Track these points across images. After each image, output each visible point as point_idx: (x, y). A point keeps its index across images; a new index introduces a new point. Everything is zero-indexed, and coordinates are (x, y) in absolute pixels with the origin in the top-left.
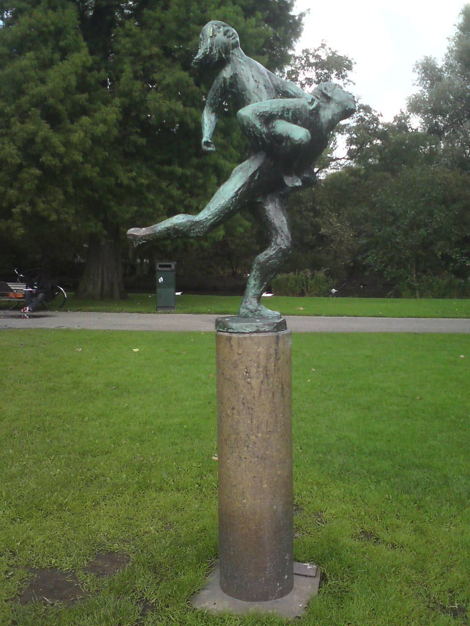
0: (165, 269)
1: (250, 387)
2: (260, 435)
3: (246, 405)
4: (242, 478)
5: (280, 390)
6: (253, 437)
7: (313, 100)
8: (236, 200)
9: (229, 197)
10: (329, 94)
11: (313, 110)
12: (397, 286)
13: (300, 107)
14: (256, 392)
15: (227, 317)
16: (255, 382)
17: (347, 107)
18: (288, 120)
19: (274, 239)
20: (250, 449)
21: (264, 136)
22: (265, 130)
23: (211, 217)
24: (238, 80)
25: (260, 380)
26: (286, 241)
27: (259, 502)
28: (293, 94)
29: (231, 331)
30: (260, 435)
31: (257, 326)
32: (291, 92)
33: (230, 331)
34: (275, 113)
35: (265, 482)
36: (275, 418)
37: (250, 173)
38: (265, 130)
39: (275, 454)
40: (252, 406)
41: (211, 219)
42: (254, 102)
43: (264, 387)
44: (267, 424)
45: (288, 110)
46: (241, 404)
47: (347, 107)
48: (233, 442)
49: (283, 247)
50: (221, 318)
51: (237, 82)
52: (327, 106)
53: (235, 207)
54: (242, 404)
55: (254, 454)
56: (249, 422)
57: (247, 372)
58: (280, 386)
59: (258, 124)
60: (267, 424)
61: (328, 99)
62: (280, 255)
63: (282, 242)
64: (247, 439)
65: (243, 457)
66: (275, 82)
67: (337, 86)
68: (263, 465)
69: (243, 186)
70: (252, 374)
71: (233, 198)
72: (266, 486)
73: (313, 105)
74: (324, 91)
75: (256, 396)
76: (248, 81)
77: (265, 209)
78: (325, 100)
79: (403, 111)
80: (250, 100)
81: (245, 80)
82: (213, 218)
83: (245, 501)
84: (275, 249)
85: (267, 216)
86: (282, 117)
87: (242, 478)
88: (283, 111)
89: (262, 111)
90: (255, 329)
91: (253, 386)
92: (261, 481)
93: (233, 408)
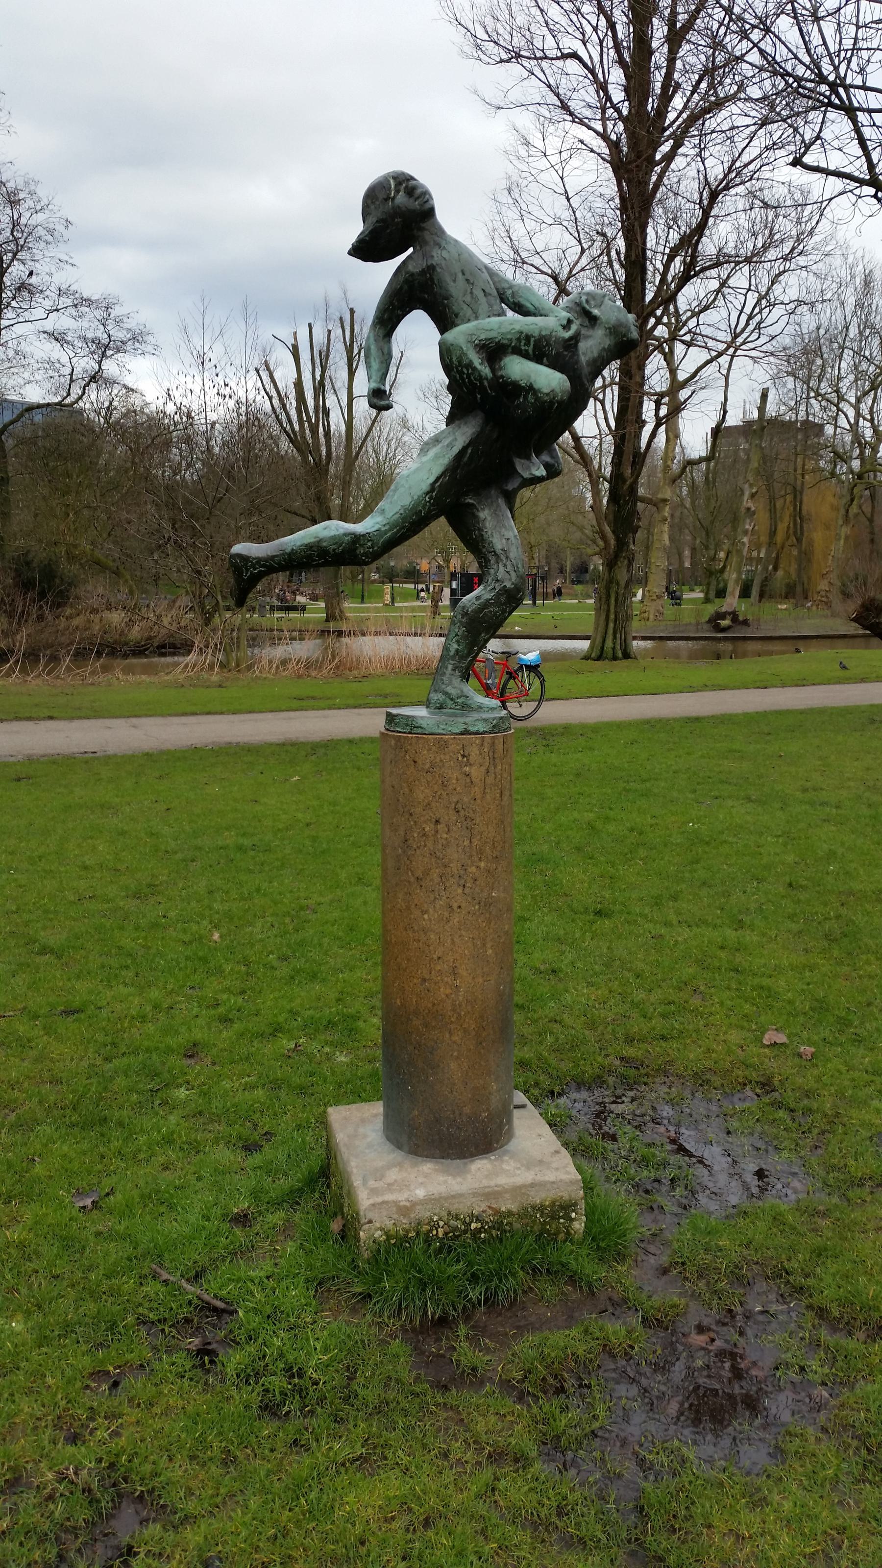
1: (468, 780)
2: (482, 865)
3: (462, 813)
4: (453, 942)
6: (473, 869)
7: (570, 322)
8: (430, 498)
9: (419, 493)
10: (596, 312)
11: (571, 338)
13: (548, 333)
14: (477, 790)
16: (476, 773)
18: (526, 356)
19: (492, 571)
20: (467, 891)
21: (486, 383)
22: (486, 371)
23: (387, 527)
24: (435, 278)
25: (483, 769)
26: (513, 574)
28: (531, 308)
29: (420, 731)
30: (482, 865)
31: (465, 723)
32: (529, 305)
33: (415, 730)
34: (506, 342)
35: (489, 945)
37: (456, 450)
38: (486, 371)
40: (471, 815)
41: (386, 532)
42: (463, 322)
43: (490, 780)
45: (528, 338)
46: (452, 812)
47: (624, 336)
48: (437, 880)
49: (509, 585)
51: (433, 282)
52: (590, 332)
53: (430, 511)
55: (474, 898)
56: (467, 843)
57: (463, 756)
59: (476, 360)
61: (592, 320)
62: (503, 599)
63: (507, 576)
64: (462, 872)
65: (455, 905)
66: (499, 286)
67: (572, 1136)
69: (443, 474)
70: (472, 761)
71: (427, 493)
73: (569, 329)
74: (587, 307)
75: (478, 796)
76: (454, 281)
77: (477, 517)
78: (587, 323)
79: (90, 335)
80: (456, 315)
81: (448, 279)
82: (391, 529)
84: (494, 588)
85: (480, 529)
86: (518, 351)
87: (453, 942)
88: (519, 340)
89: (483, 337)
90: (462, 728)
91: (474, 780)
92: (484, 945)
93: (437, 822)
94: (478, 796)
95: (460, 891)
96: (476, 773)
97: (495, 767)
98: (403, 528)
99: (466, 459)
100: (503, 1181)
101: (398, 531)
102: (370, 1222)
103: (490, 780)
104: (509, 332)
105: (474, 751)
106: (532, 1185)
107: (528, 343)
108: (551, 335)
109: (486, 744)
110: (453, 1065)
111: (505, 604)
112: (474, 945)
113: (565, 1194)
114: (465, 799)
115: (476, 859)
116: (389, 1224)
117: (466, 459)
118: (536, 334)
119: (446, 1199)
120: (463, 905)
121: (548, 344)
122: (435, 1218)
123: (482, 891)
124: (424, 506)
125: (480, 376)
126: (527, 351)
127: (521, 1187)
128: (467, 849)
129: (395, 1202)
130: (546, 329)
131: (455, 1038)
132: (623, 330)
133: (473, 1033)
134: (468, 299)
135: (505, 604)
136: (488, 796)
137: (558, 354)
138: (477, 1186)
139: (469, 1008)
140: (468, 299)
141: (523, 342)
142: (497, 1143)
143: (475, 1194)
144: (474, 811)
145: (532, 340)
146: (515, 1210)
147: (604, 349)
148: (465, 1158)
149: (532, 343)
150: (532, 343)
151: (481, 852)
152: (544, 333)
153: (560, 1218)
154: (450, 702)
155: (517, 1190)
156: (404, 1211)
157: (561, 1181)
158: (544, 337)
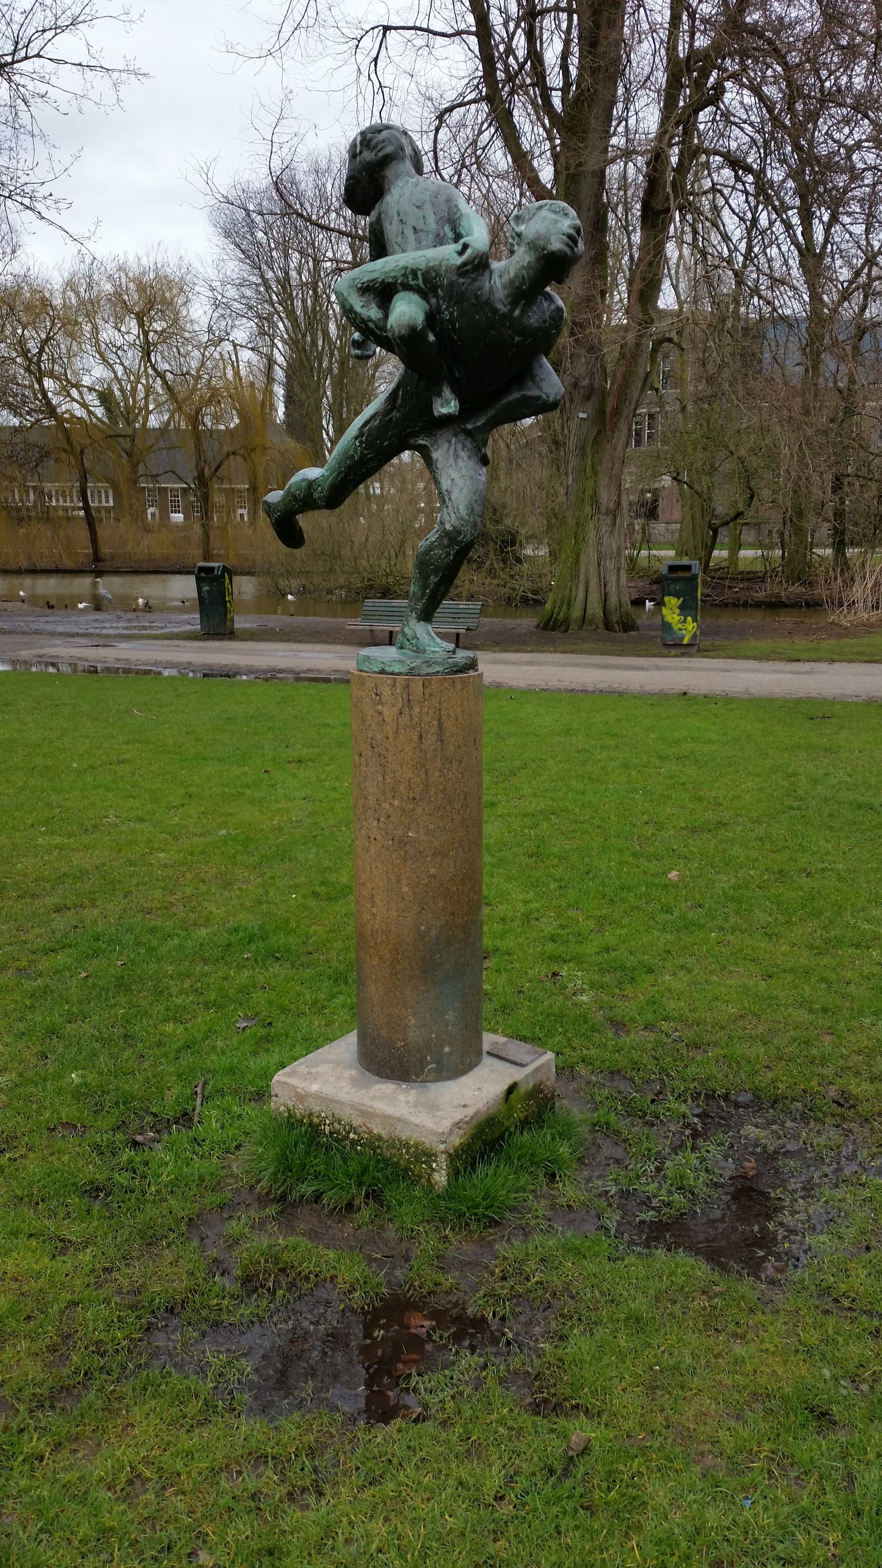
0: (680, 574)
2: (396, 803)
3: (376, 749)
5: (435, 729)
6: (387, 805)
8: (361, 442)
12: (48, 945)
13: (437, 263)
14: (389, 730)
15: (161, 628)
16: (389, 712)
17: (544, 249)
20: (381, 825)
25: (396, 710)
27: (395, 914)
30: (396, 803)
34: (390, 280)
35: (404, 882)
36: (424, 776)
39: (423, 837)
43: (404, 720)
44: (409, 785)
45: (414, 272)
47: (544, 249)
49: (448, 527)
50: (54, 646)
54: (369, 747)
56: (380, 779)
57: (376, 695)
58: (436, 723)
60: (409, 785)
68: (402, 853)
70: (384, 700)
71: (356, 438)
72: (406, 889)
75: (391, 735)
82: (331, 474)
83: (374, 910)
88: (405, 275)
89: (365, 279)
94: (391, 735)
95: (375, 824)
96: (387, 711)
97: (411, 709)
98: (341, 472)
99: (399, 401)
100: (381, 1106)
101: (337, 476)
102: (276, 1096)
103: (404, 720)
104: (393, 270)
105: (386, 691)
106: (399, 1119)
107: (415, 277)
108: (440, 265)
109: (398, 685)
110: (373, 987)
111: (448, 546)
112: (389, 879)
113: (429, 1141)
114: (379, 737)
115: (389, 796)
116: (291, 1104)
117: (399, 401)
118: (423, 266)
119: (336, 1102)
120: (378, 838)
121: (438, 275)
122: (323, 1115)
123: (395, 828)
124: (355, 451)
125: (363, 319)
126: (418, 285)
127: (390, 1117)
128: (381, 785)
129: (295, 1088)
130: (434, 259)
131: (374, 963)
132: (542, 243)
133: (388, 963)
134: (399, 239)
135: (448, 546)
136: (401, 737)
137: (451, 284)
138: (356, 1100)
139: (384, 938)
140: (399, 239)
141: (410, 277)
142: (418, 1076)
143: (353, 1107)
144: (387, 749)
145: (419, 273)
146: (385, 1137)
147: (523, 267)
148: (381, 1077)
149: (420, 277)
150: (420, 277)
151: (394, 790)
152: (431, 264)
153: (422, 1163)
154: (407, 643)
155: (387, 1119)
156: (301, 1097)
157: (423, 1126)
158: (432, 268)
